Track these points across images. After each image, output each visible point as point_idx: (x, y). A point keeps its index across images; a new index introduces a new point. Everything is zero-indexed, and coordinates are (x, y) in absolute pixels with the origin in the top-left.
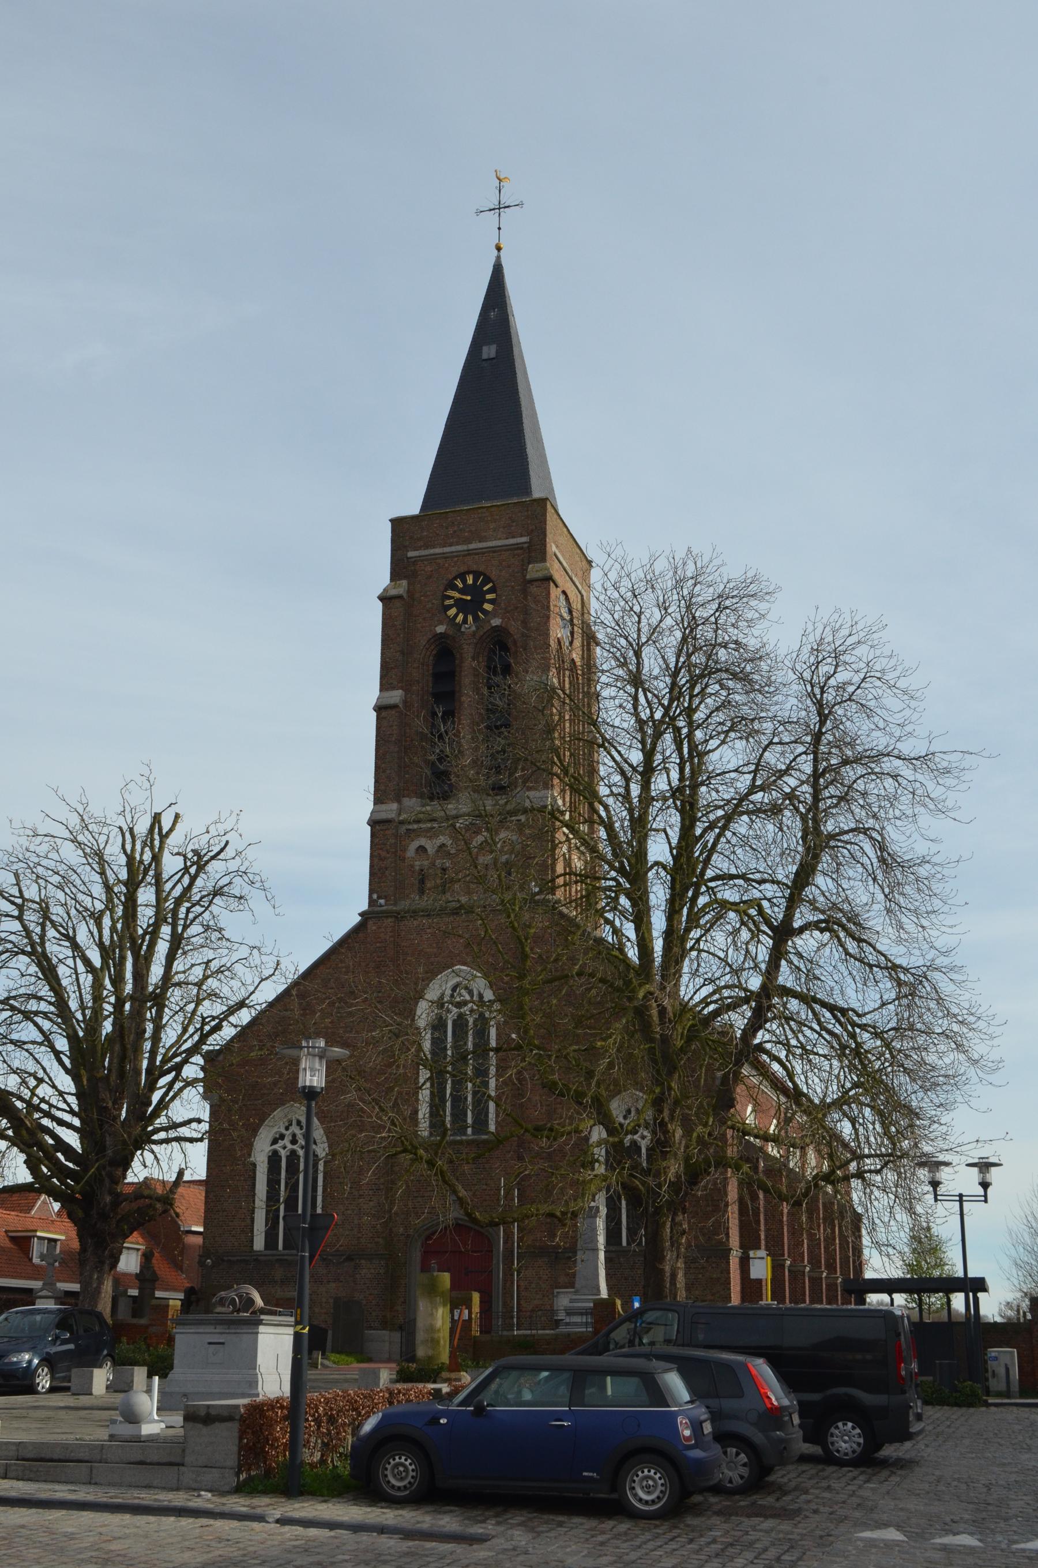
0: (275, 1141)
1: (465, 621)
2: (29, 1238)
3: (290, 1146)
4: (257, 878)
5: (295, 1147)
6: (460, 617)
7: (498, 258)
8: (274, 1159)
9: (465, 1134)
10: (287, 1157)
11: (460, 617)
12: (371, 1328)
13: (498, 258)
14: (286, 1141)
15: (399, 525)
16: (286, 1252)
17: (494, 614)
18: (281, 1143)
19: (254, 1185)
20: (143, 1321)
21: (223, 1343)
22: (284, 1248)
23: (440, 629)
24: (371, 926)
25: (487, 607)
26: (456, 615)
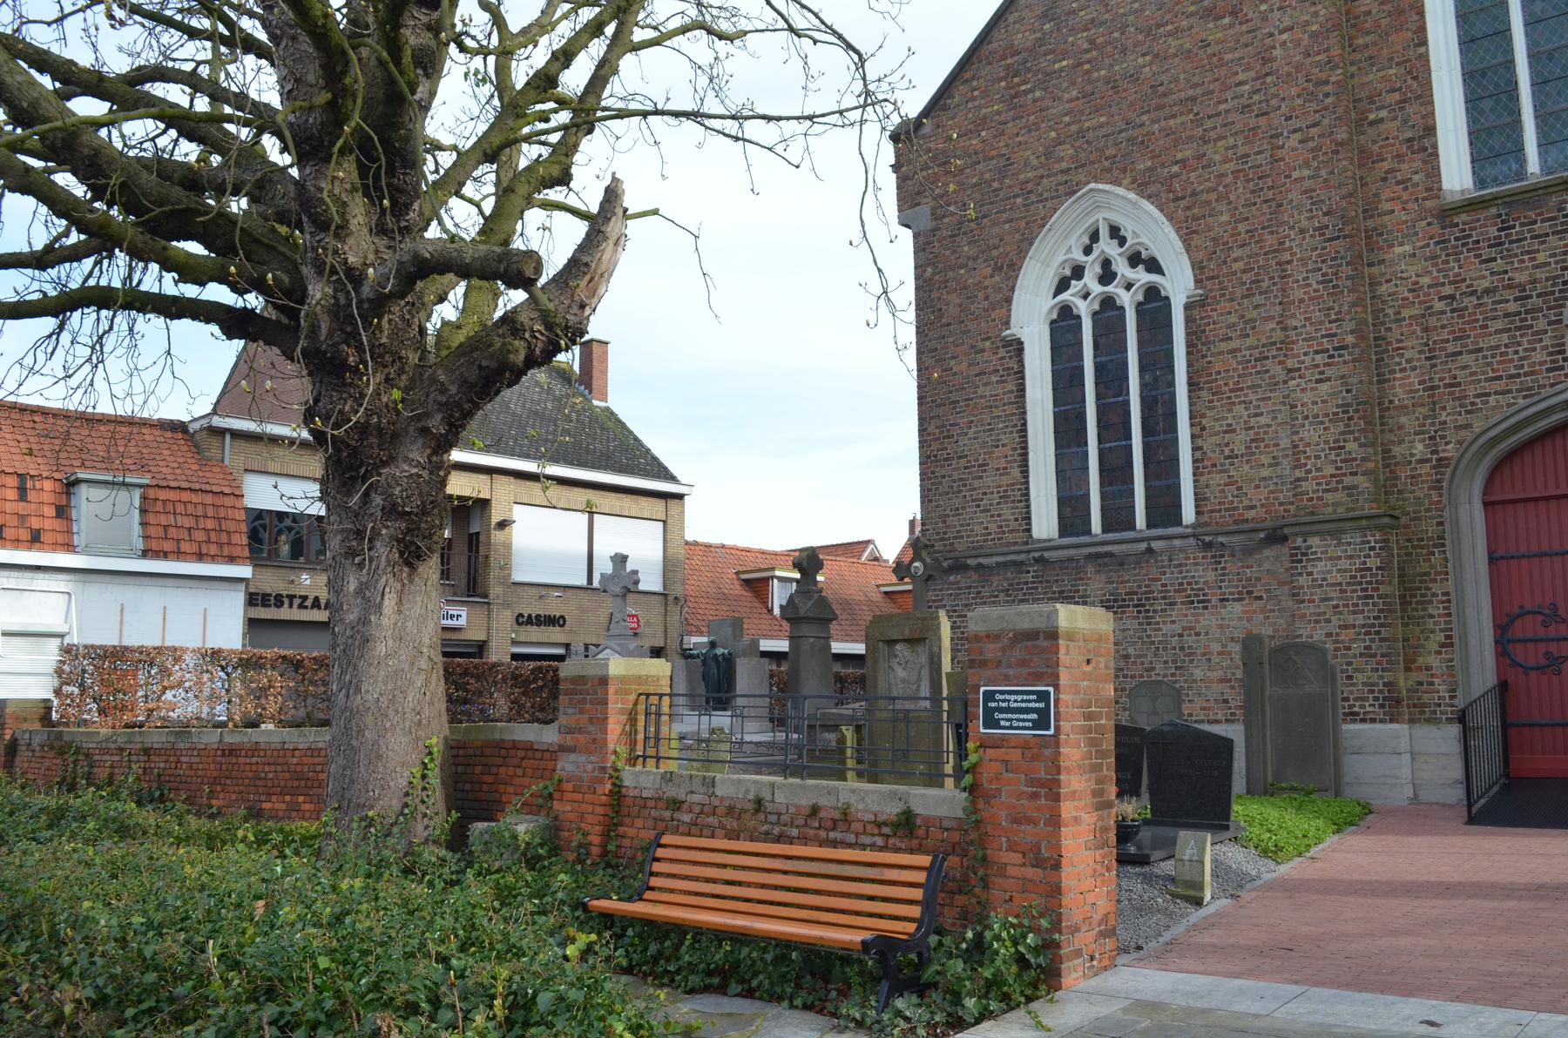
0: (1062, 286)
2: (766, 581)
5: (1109, 288)
8: (1064, 325)
12: (1353, 716)
14: (1090, 280)
18: (1076, 286)
19: (1022, 389)
20: (548, 735)
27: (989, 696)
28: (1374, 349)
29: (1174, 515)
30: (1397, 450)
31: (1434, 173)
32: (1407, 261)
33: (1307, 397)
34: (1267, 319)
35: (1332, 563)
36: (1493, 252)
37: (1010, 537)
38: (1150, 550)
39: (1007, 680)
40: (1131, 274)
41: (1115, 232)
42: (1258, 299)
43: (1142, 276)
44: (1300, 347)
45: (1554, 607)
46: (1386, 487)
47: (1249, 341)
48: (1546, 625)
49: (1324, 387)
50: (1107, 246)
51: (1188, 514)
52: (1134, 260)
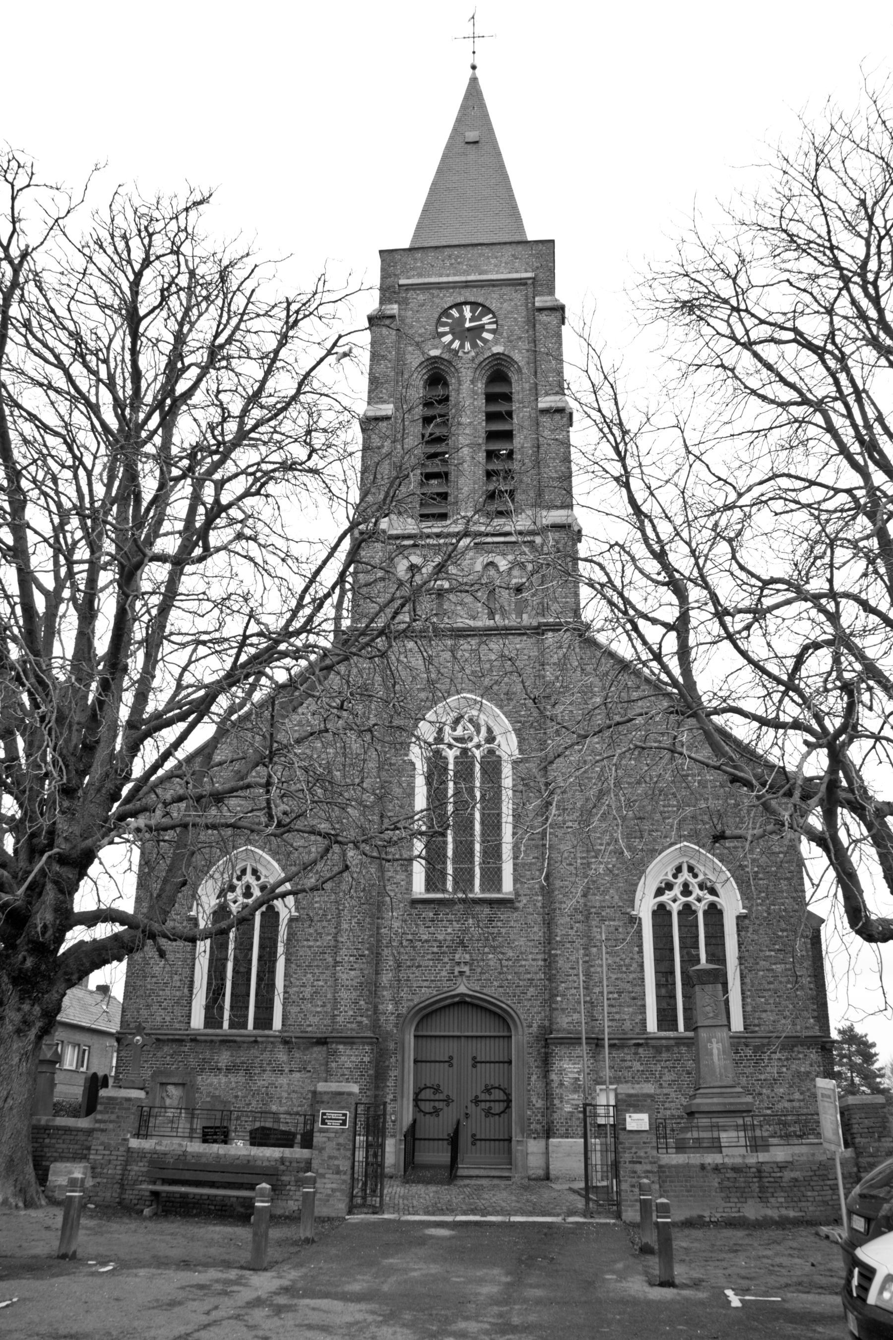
0: (660, 892)
1: (462, 346)
3: (241, 899)
8: (661, 913)
10: (680, 913)
15: (389, 258)
16: (234, 1031)
17: (496, 342)
18: (230, 896)
22: (231, 1026)
23: (434, 353)
26: (452, 342)
27: (324, 1114)
29: (269, 1024)
30: (380, 1007)
31: (410, 883)
32: (394, 921)
33: (344, 976)
34: (329, 934)
35: (350, 1058)
36: (430, 924)
37: (177, 1026)
38: (256, 1042)
39: (331, 1108)
41: (255, 872)
42: (325, 924)
44: (343, 952)
45: (439, 1086)
46: (375, 1025)
47: (318, 943)
48: (434, 1094)
49: (352, 973)
51: (277, 1024)
52: (701, 886)
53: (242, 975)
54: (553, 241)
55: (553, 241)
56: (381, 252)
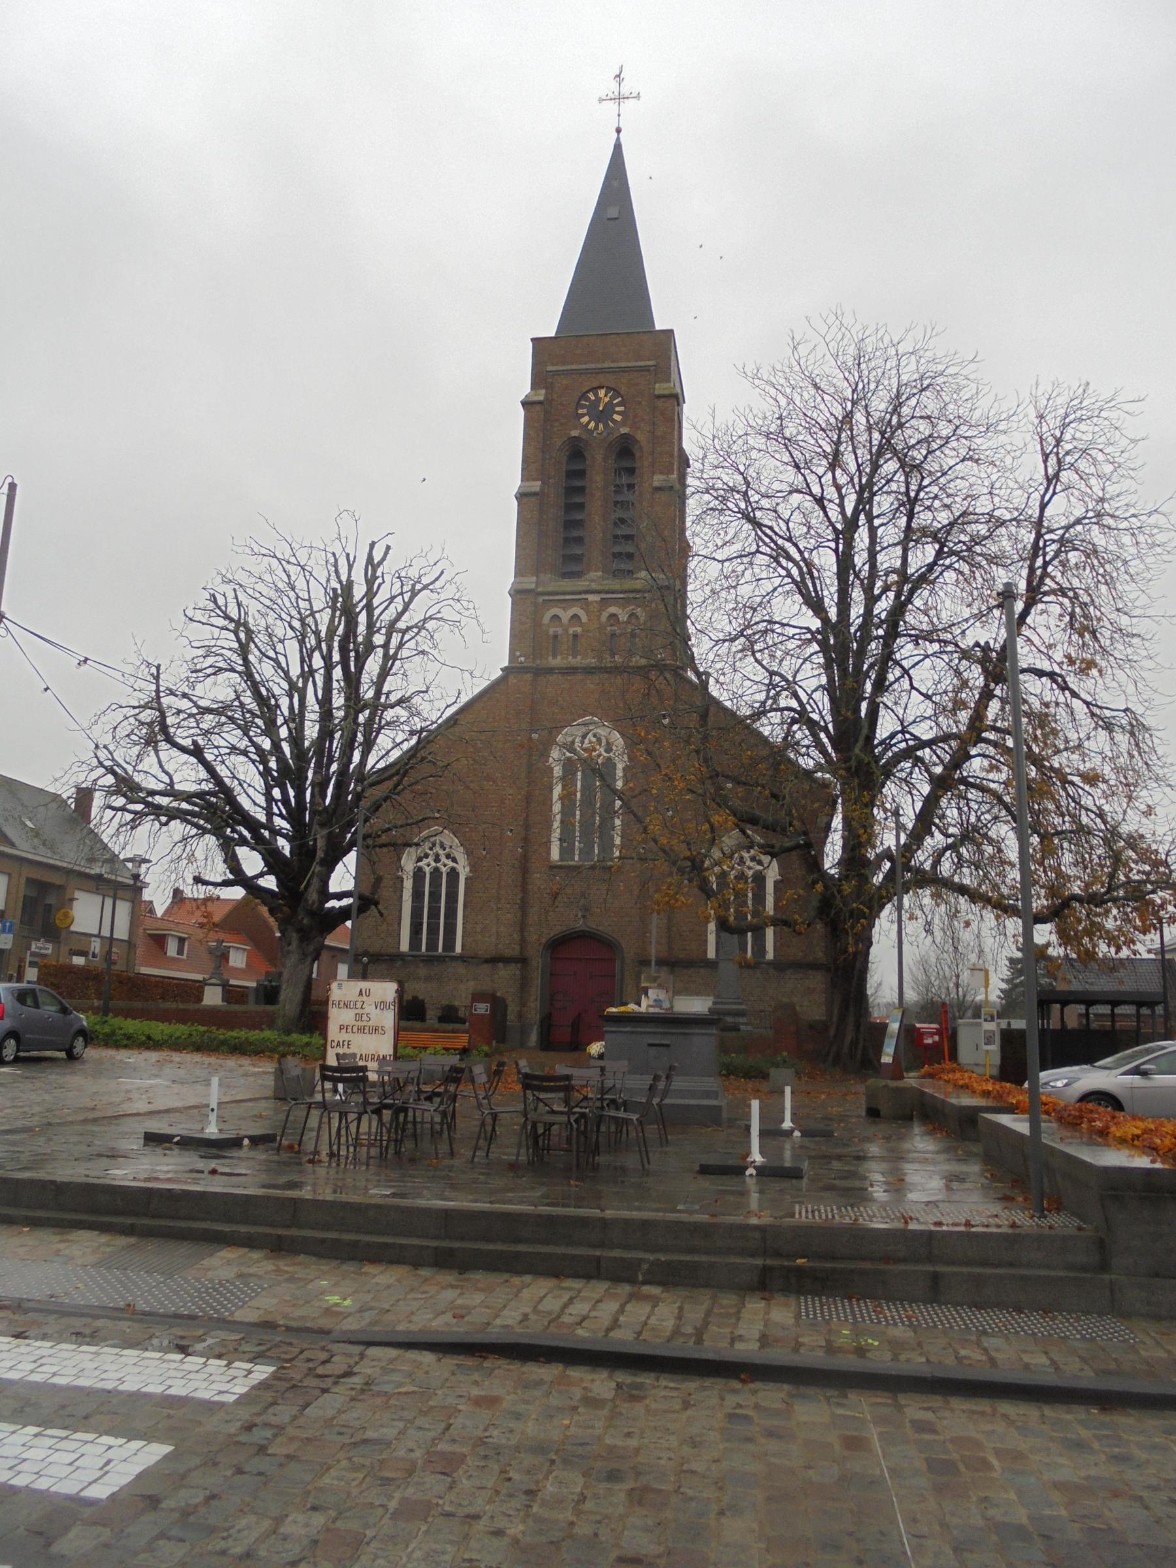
0: (419, 859)
1: (596, 427)
3: (433, 864)
4: (471, 606)
6: (592, 425)
7: (618, 138)
8: (418, 874)
9: (573, 859)
10: (448, 874)
11: (592, 425)
13: (618, 138)
14: (430, 860)
18: (425, 861)
21: (668, 1046)
22: (427, 950)
23: (575, 433)
24: (512, 680)
25: (617, 417)
26: (589, 423)
28: (524, 907)
29: (453, 948)
32: (538, 879)
40: (447, 861)
43: (451, 864)
44: (503, 901)
50: (438, 849)
52: (448, 856)
53: (434, 914)
54: (672, 331)
55: (672, 331)
56: (532, 340)
